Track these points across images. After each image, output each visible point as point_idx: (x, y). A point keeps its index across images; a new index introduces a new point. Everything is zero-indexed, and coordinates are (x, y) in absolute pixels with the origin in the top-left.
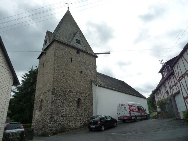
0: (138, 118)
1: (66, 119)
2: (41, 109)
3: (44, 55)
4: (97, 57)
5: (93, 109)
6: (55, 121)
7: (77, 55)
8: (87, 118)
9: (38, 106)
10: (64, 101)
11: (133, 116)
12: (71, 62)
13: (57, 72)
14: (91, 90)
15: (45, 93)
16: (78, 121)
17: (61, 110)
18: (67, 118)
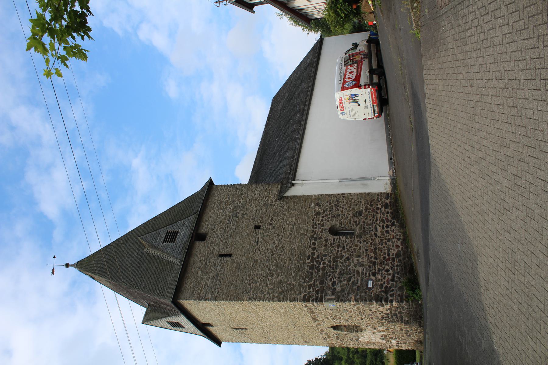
0: (374, 66)
1: (381, 263)
2: (356, 329)
3: (210, 328)
4: (47, 77)
5: (357, 194)
6: (386, 292)
7: (209, 241)
8: (378, 209)
9: (350, 335)
10: (338, 270)
11: (371, 79)
12: (230, 255)
13: (262, 292)
14: (306, 199)
15: (316, 320)
16: (387, 232)
17: (360, 279)
18: (378, 261)
